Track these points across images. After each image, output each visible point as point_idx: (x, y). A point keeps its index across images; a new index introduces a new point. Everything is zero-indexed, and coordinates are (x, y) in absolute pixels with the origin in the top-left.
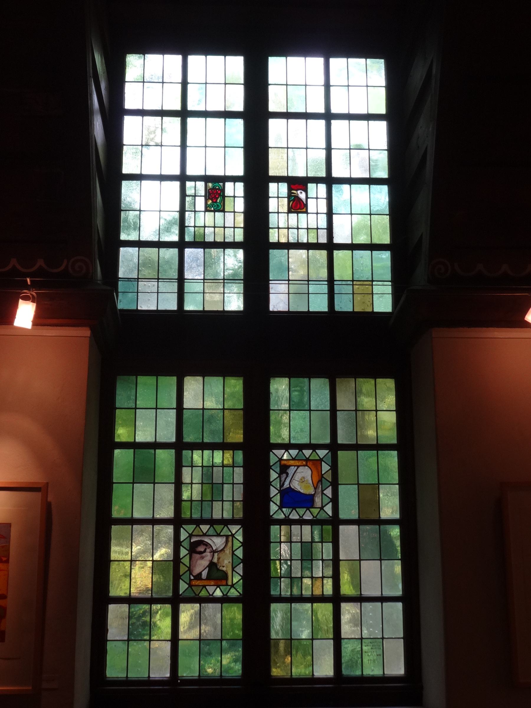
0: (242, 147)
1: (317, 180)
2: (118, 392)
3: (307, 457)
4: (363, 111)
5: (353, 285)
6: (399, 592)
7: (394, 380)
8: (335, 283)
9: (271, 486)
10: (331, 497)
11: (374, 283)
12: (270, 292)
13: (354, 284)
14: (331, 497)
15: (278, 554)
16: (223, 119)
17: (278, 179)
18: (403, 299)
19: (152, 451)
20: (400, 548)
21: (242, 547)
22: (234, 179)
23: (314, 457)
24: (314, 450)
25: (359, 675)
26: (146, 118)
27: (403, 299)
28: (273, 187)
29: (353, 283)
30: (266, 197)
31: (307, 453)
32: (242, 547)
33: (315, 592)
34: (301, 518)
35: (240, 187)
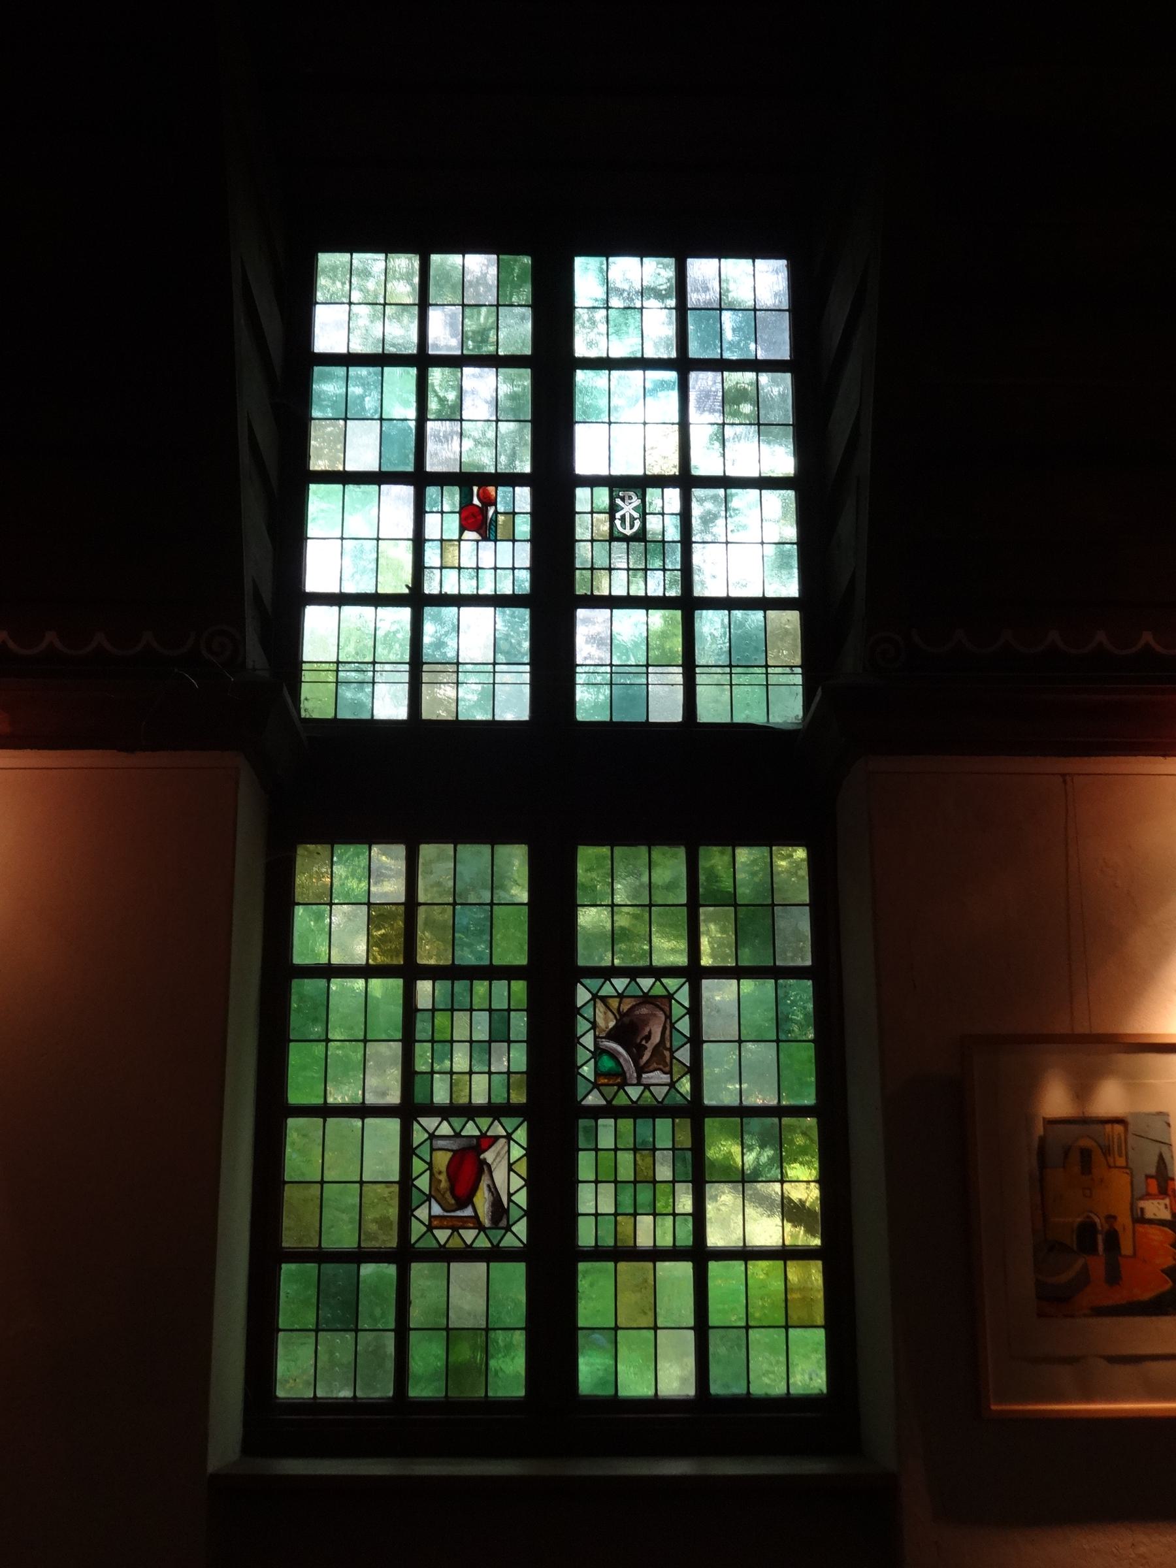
0: (527, 541)
1: (661, 482)
2: (281, 1351)
3: (646, 991)
4: (753, 473)
5: (731, 674)
6: (809, 1100)
7: (805, 848)
8: (305, 666)
9: (578, 984)
10: (689, 1036)
11: (378, 667)
12: (577, 682)
13: (733, 672)
14: (689, 1036)
15: (596, 419)
16: (493, 609)
17: (593, 482)
18: (817, 699)
19: (357, 1123)
20: (812, 1006)
21: (525, 1188)
22: (513, 480)
23: (658, 990)
24: (658, 979)
25: (742, 1394)
26: (347, 610)
27: (817, 699)
28: (582, 495)
29: (731, 670)
30: (569, 513)
31: (646, 983)
32: (525, 1188)
33: (660, 1220)
34: (635, 1105)
35: (523, 496)
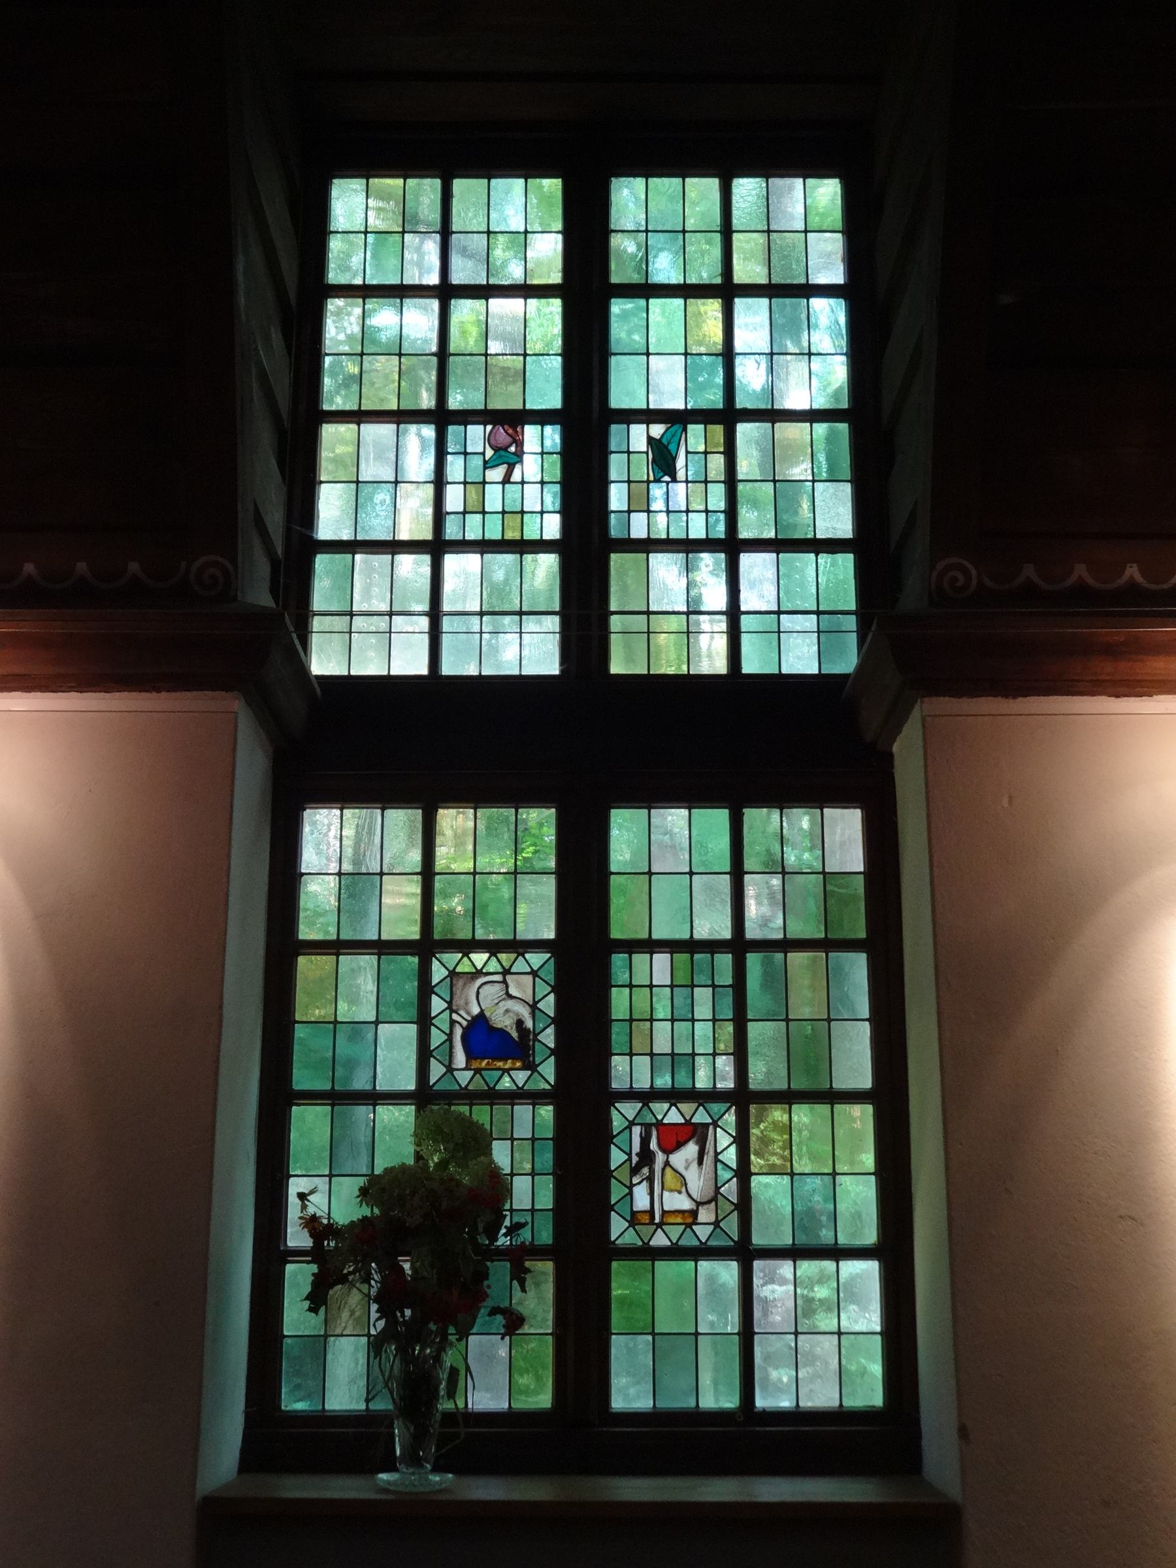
22: (542, 417)
